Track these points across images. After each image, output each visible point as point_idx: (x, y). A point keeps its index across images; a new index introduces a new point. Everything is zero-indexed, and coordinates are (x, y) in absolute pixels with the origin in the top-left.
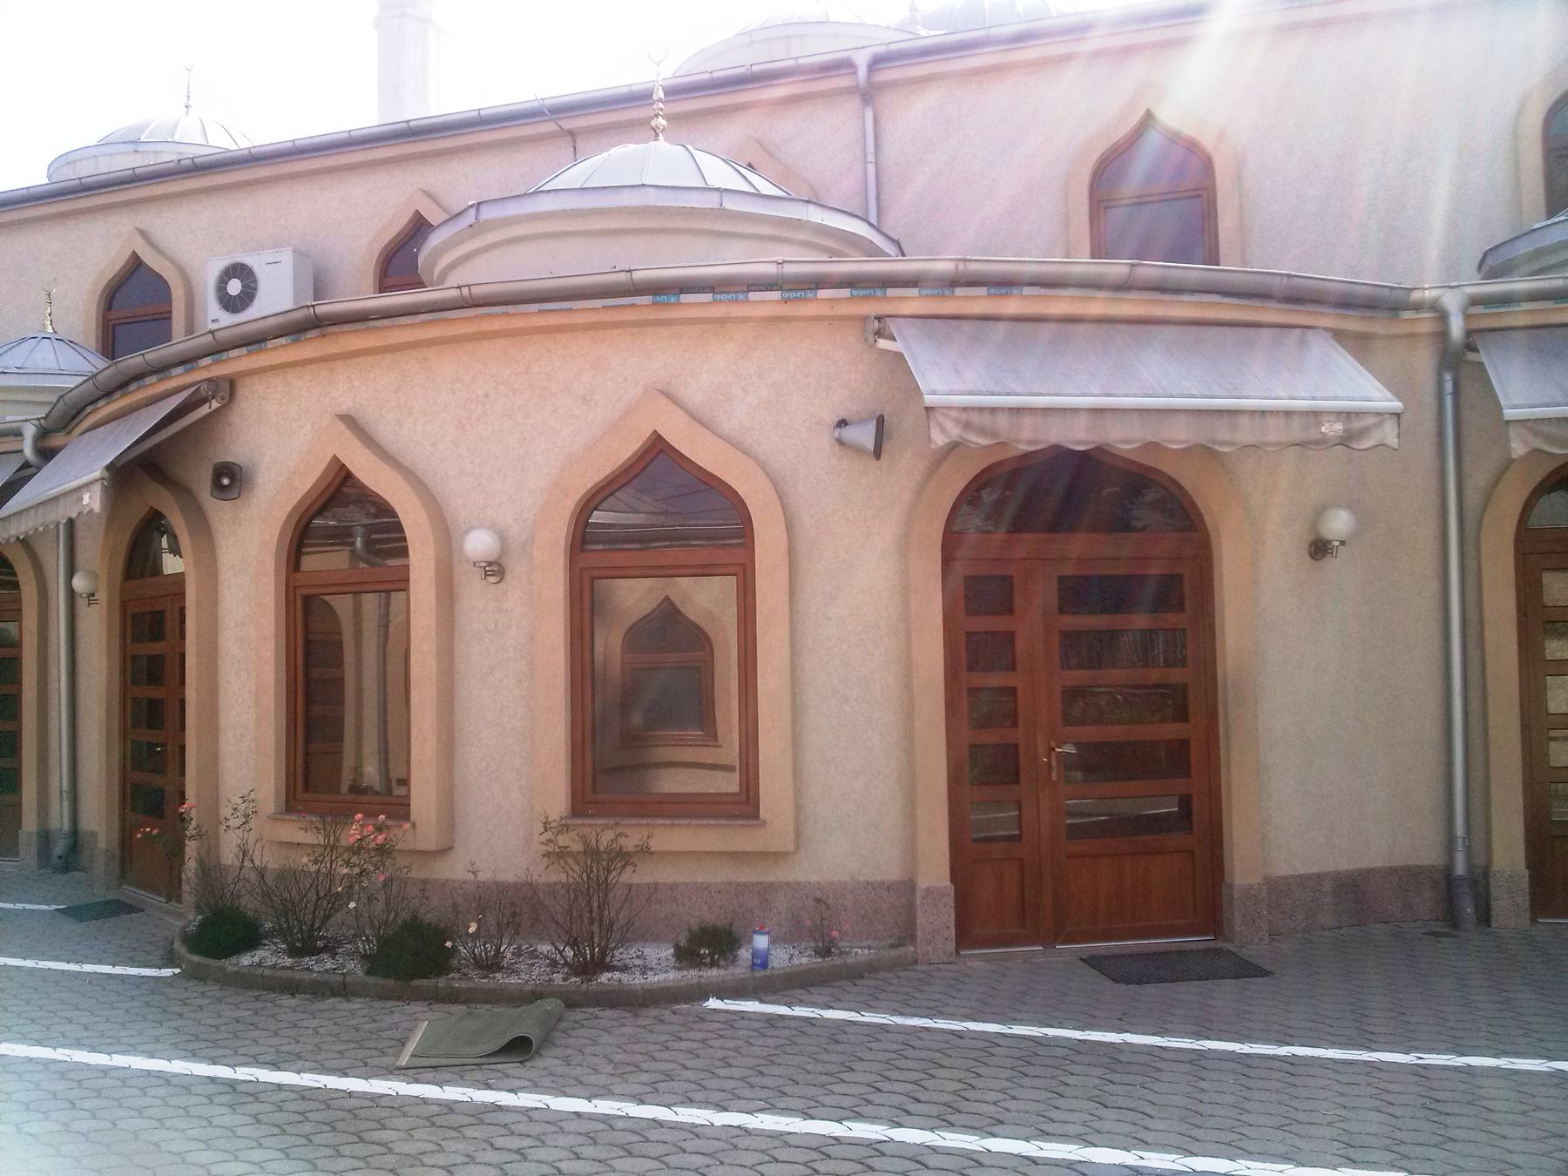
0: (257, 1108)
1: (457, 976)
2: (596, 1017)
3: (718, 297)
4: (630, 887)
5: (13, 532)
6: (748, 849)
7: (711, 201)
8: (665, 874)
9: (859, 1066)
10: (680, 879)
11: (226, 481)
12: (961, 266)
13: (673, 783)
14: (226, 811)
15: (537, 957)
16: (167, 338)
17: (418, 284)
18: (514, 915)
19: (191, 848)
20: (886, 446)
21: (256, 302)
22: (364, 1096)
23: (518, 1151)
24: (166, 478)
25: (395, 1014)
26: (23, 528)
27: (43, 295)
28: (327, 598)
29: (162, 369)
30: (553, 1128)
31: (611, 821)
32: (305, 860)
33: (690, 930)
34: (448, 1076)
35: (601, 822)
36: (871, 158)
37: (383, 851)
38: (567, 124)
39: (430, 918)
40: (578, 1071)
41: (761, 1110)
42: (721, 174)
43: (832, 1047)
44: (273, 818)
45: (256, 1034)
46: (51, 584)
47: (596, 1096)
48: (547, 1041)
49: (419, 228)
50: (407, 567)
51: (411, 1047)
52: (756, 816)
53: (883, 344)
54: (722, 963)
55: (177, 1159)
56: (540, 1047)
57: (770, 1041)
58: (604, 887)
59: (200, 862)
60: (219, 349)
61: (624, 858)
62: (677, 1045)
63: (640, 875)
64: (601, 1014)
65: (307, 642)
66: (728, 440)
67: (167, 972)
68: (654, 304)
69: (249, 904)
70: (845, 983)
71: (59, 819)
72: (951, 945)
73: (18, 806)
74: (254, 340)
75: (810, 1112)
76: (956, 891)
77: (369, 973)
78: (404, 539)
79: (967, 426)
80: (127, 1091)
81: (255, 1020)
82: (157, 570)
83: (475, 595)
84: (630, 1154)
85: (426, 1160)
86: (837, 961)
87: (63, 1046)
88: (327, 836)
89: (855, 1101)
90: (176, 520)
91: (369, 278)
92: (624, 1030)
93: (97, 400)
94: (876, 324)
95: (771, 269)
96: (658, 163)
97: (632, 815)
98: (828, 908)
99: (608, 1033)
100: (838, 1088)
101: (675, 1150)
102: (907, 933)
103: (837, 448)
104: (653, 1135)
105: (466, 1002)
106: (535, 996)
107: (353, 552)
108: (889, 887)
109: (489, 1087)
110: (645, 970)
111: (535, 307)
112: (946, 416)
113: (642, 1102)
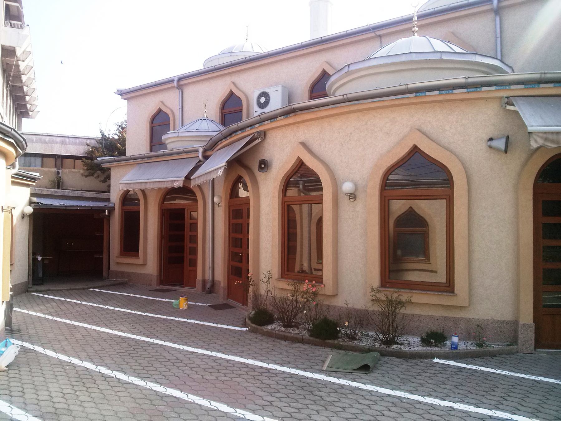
0: (277, 379)
1: (341, 340)
2: (392, 361)
3: (441, 92)
4: (403, 315)
5: (197, 183)
6: (449, 304)
7: (437, 57)
8: (417, 311)
9: (497, 390)
10: (422, 313)
11: (263, 166)
12: (543, 76)
13: (412, 277)
14: (262, 277)
15: (369, 336)
16: (241, 119)
17: (326, 95)
18: (361, 321)
19: (251, 289)
20: (509, 148)
21: (269, 105)
22: (312, 379)
23: (368, 405)
24: (244, 166)
25: (321, 351)
26: (200, 182)
27: (203, 106)
28: (292, 206)
29: (242, 129)
30: (380, 399)
31: (396, 290)
32: (289, 295)
33: (427, 333)
34: (341, 375)
35: (392, 290)
36: (498, 35)
37: (315, 294)
38: (378, 33)
39: (331, 318)
40: (387, 379)
41: (459, 402)
42: (440, 46)
43: (485, 381)
44: (277, 280)
45: (274, 353)
46: (207, 200)
47: (395, 389)
48: (375, 367)
49: (324, 76)
50: (322, 195)
51: (327, 363)
53: (509, 107)
54: (439, 345)
55: (252, 393)
56: (373, 369)
57: (460, 377)
58: (394, 314)
59: (254, 293)
60: (261, 122)
61: (402, 304)
62: (424, 374)
63: (407, 311)
64: (394, 359)
65: (288, 220)
66: (444, 147)
67: (244, 329)
68: (416, 96)
69: (270, 308)
70: (489, 358)
71: (208, 277)
72: (533, 346)
73: (196, 271)
74: (273, 118)
75: (478, 405)
76: (535, 326)
77: (311, 336)
78: (321, 185)
79: (546, 139)
80: (235, 368)
81: (274, 348)
82: (237, 196)
83: (346, 205)
84: (409, 412)
85: (336, 404)
86: (486, 349)
87: (214, 351)
88: (295, 287)
89: (496, 403)
90: (247, 179)
91: (307, 95)
92: (403, 366)
93: (222, 140)
94: (506, 100)
95: (463, 81)
96: (417, 43)
97: (404, 289)
98: (482, 328)
99: (399, 367)
100: (488, 397)
101: (426, 412)
102: (514, 341)
103: (489, 149)
104: (418, 406)
105: (345, 350)
106: (369, 351)
107: (299, 190)
108: (507, 323)
109: (356, 381)
110: (409, 345)
112: (538, 136)
113: (412, 394)
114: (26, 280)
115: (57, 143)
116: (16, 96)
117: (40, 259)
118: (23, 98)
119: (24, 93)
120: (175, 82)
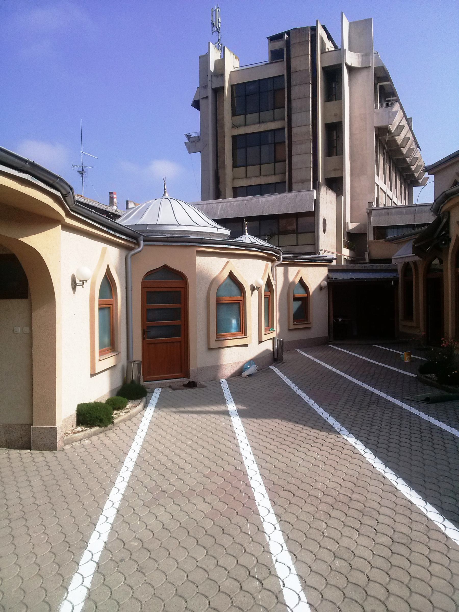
114: (327, 335)
115: (425, 212)
116: (402, 168)
117: (340, 320)
118: (409, 168)
119: (408, 163)
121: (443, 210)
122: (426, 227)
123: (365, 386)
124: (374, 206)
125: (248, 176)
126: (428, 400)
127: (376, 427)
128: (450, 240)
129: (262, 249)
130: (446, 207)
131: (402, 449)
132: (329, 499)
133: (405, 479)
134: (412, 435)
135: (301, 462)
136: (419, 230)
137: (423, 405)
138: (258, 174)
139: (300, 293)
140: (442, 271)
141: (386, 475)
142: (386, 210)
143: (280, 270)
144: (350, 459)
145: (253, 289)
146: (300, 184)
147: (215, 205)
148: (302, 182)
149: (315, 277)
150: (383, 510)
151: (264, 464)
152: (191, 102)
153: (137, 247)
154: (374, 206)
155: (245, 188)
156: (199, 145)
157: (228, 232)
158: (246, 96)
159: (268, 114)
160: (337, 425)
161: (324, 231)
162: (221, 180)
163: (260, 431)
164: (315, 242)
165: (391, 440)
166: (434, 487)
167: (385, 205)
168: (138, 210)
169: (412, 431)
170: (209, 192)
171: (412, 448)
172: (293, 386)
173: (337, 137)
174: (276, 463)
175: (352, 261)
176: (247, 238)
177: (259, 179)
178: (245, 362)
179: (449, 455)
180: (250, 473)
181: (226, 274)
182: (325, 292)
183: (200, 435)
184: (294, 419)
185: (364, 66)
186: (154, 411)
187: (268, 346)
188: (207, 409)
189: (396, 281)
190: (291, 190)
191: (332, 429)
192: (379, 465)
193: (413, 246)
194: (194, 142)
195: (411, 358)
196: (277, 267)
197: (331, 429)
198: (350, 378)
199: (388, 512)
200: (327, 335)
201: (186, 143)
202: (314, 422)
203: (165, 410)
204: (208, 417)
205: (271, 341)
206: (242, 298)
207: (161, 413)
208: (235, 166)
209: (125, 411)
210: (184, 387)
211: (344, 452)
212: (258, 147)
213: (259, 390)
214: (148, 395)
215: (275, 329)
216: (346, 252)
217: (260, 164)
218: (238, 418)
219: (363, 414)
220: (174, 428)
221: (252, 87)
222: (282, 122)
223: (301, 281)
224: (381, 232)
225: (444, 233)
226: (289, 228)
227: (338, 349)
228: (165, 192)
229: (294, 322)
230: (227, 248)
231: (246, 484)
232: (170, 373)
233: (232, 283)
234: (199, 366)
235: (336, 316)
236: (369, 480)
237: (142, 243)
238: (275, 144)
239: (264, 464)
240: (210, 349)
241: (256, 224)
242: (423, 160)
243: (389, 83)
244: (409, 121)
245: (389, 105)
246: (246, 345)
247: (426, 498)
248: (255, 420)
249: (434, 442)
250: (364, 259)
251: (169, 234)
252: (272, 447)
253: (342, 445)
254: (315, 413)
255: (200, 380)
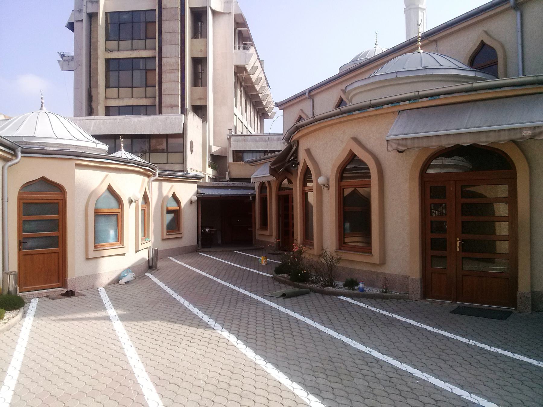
7: (394, 76)
52: (371, 253)
79: (399, 144)
86: (389, 294)
111: (327, 120)
114: (196, 243)
115: (274, 140)
117: (207, 230)
120: (307, 94)
121: (293, 139)
122: (281, 152)
123: (231, 286)
124: (233, 133)
125: (134, 96)
126: (284, 296)
127: (245, 321)
128: (299, 164)
129: (139, 165)
130: (295, 137)
131: (267, 338)
132: (211, 388)
133: (272, 363)
134: (274, 326)
135: (182, 357)
136: (273, 155)
137: (280, 300)
138: (130, 96)
139: (173, 206)
140: (292, 189)
141: (257, 362)
142: (243, 137)
143: (156, 185)
144: (225, 351)
145: (131, 202)
146: (170, 108)
147: (88, 121)
148: (172, 106)
149: (187, 193)
150: (258, 392)
151: (148, 362)
152: (66, 23)
153: (14, 158)
154: (233, 133)
155: (117, 108)
156: (72, 64)
157: (106, 147)
158: (119, 24)
159: (141, 43)
160: (211, 322)
161: (192, 152)
162: (94, 98)
163: (142, 333)
164: (183, 162)
165: (258, 331)
166: (297, 368)
167: (242, 133)
168: (15, 121)
169: (274, 323)
170: (82, 108)
171: (276, 336)
172: (169, 290)
173: (202, 71)
174: (160, 360)
175: (215, 179)
176: (123, 154)
177: (131, 100)
178: (122, 271)
179: (305, 340)
180: (136, 371)
181: (105, 187)
182: (195, 206)
183: (83, 341)
184: (173, 320)
185: (226, 12)
186: (34, 321)
187: (144, 255)
188: (87, 315)
189: (254, 197)
190: (161, 112)
191: (208, 326)
192: (250, 353)
193: (270, 167)
194: (67, 61)
195: (267, 261)
196: (153, 183)
197: (206, 326)
198: (219, 280)
199: (262, 393)
200: (196, 244)
201: (59, 61)
202: (190, 321)
203: (44, 318)
204: (89, 323)
205: (147, 250)
206: (120, 210)
207: (40, 322)
208: (107, 87)
209: (3, 321)
210: (61, 297)
211: (220, 344)
212: (117, 73)
213: (137, 294)
214: (26, 305)
215: (150, 239)
216: (210, 172)
217: (132, 87)
218: (119, 322)
219: (233, 311)
220: (56, 336)
221: (125, 17)
222: (154, 51)
223: (174, 196)
224: (238, 155)
225: (292, 158)
226: (158, 147)
227: (206, 255)
228: (42, 105)
229: (167, 232)
230: (100, 163)
231: (134, 381)
232: (46, 284)
233: (110, 196)
234: (77, 276)
235: (203, 227)
236: (243, 367)
237: (20, 155)
238: (147, 70)
239: (148, 362)
240: (88, 259)
241: (129, 141)
242: (272, 97)
243: (246, 29)
244: (261, 62)
245: (246, 48)
246: (124, 254)
247: (292, 377)
248: (136, 323)
249: (292, 330)
250: (225, 178)
251: (46, 146)
252: (154, 346)
253: (217, 339)
254: (191, 313)
255: (78, 289)
